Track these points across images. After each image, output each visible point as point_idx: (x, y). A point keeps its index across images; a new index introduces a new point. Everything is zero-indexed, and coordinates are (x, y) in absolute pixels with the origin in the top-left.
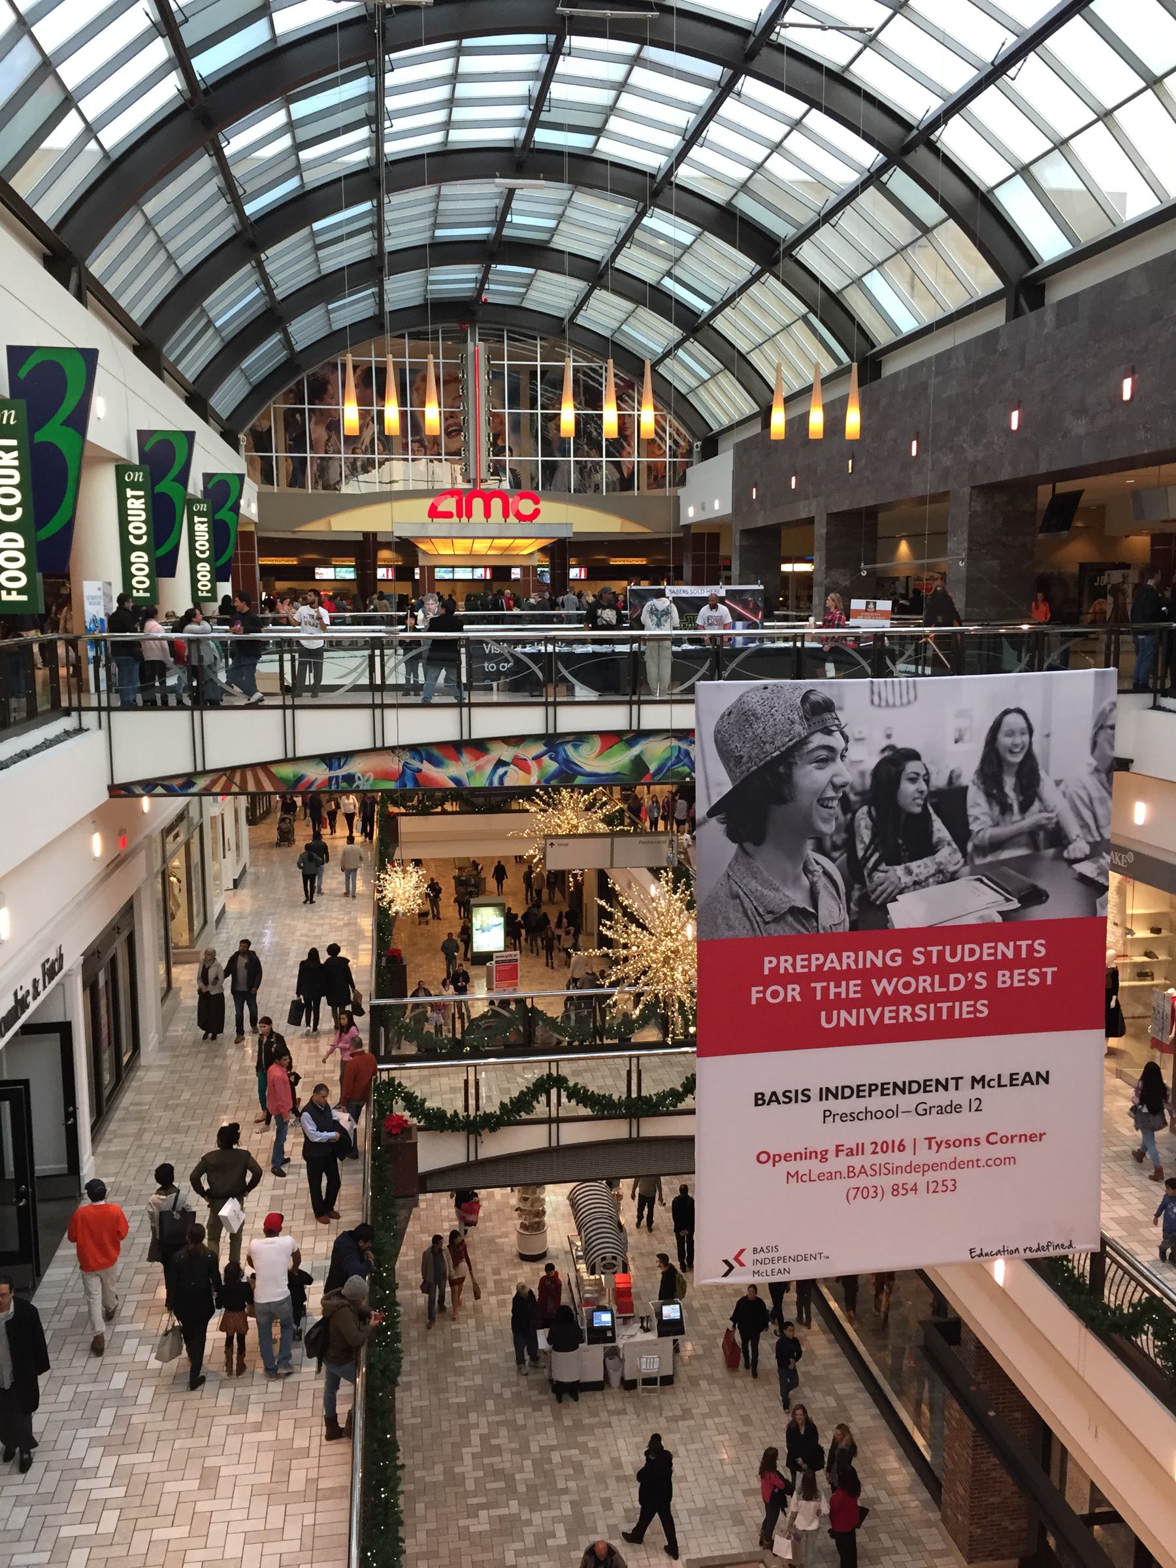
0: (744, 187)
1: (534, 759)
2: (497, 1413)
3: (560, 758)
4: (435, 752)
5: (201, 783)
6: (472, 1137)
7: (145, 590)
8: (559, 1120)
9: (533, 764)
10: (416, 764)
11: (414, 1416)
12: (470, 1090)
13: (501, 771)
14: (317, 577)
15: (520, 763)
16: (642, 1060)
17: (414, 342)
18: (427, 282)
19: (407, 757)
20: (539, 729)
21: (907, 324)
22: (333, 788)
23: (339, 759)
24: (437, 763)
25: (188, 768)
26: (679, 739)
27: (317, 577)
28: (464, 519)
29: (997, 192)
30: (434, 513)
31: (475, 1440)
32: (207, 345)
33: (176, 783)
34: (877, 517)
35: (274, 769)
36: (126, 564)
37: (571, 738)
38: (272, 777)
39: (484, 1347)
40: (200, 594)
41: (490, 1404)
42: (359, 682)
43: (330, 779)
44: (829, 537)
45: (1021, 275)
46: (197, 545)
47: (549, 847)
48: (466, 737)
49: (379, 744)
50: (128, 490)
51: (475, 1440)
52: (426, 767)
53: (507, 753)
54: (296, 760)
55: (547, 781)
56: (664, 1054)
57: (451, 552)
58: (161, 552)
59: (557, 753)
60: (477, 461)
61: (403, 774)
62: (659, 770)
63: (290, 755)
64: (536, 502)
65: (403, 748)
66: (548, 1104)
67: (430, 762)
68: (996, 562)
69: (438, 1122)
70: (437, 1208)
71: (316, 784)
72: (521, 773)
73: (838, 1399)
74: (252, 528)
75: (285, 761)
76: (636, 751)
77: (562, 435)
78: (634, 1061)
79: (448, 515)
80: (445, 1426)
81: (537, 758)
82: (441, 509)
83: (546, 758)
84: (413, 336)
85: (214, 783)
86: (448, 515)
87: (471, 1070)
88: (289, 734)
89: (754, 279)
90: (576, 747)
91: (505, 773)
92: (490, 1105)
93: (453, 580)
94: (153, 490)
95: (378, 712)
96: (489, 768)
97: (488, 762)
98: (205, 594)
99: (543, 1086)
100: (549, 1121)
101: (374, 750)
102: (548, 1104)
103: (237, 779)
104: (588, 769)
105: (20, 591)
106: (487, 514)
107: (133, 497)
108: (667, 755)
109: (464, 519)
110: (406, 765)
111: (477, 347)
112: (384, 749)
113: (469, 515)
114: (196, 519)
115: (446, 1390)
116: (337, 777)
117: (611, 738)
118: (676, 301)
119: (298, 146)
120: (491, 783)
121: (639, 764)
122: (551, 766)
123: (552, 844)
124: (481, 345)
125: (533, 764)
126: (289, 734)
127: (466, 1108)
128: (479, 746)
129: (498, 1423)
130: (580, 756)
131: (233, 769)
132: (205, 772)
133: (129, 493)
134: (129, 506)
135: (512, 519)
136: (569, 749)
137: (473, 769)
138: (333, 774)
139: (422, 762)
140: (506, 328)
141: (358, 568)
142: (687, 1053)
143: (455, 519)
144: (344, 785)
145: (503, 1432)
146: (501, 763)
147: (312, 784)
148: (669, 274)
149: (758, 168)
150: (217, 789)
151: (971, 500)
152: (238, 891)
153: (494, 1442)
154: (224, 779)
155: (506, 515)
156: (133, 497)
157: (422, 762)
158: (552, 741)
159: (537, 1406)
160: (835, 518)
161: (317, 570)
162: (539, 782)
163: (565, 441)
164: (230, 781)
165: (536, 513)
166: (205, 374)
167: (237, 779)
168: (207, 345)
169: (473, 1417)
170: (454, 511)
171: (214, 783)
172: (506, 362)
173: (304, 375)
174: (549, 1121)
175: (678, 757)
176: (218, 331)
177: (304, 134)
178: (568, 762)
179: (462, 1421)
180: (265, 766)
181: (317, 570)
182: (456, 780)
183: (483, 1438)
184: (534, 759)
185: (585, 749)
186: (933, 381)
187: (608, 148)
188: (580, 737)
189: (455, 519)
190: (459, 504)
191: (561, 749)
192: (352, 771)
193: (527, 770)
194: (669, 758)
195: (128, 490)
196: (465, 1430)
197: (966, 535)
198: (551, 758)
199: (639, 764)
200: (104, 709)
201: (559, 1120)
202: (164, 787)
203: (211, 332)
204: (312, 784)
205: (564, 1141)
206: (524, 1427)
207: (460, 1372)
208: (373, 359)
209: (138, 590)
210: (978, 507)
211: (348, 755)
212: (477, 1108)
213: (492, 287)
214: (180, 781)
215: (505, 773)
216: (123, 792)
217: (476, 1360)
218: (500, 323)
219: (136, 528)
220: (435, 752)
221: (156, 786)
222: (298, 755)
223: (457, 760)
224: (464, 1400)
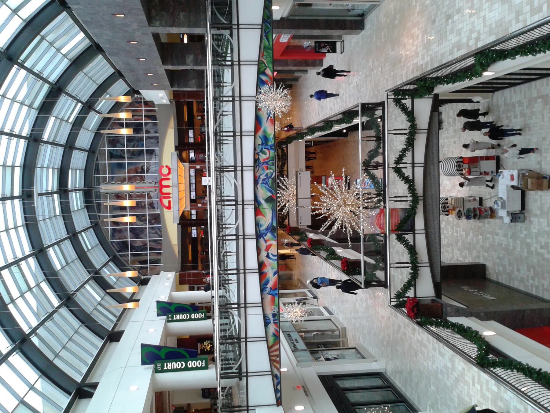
0: (30, 106)
1: (266, 243)
2: (532, 239)
3: (266, 232)
4: (263, 282)
5: (276, 372)
6: (417, 131)
7: (202, 362)
8: (413, 163)
9: (268, 243)
10: (268, 290)
11: (530, 271)
12: (398, 132)
13: (271, 256)
14: (196, 236)
15: (268, 248)
16: (391, 263)
17: (101, 172)
18: (78, 210)
19: (265, 293)
20: (254, 241)
21: (82, 35)
22: (278, 322)
23: (266, 319)
24: (268, 282)
25: (270, 377)
26: (258, 183)
27: (196, 236)
28: (171, 195)
29: (24, 18)
30: (169, 208)
31: (542, 251)
32: (108, 302)
33: (276, 381)
34: (163, 43)
35: (270, 344)
36: (192, 369)
37: (257, 228)
38: (273, 345)
39: (505, 236)
40: (204, 366)
41: (529, 241)
42: (237, 314)
43: (274, 323)
44: (173, 64)
45: (59, 5)
46: (185, 318)
47: (302, 224)
48: (257, 271)
49: (261, 305)
50: (164, 369)
51: (542, 251)
52: (270, 285)
53: (264, 254)
54: (266, 337)
55: (275, 237)
56: (387, 109)
57: (184, 198)
58: (187, 356)
59: (264, 233)
60: (148, 187)
61: (272, 294)
62: (271, 192)
63: (265, 339)
64: (163, 167)
65: (262, 295)
66: (406, 168)
67: (267, 284)
68: (181, 14)
69: (412, 283)
70: (448, 235)
71: (276, 328)
72: (272, 248)
73: (539, 97)
74: (178, 274)
75: (267, 340)
76: (263, 202)
77: (135, 205)
78: (392, 266)
79: (169, 202)
80: (535, 261)
81: (266, 241)
82: (167, 205)
83: (266, 238)
84: (99, 211)
85: (276, 367)
86: (169, 202)
87: (390, 132)
88: (257, 339)
89: (67, 94)
90: (261, 226)
91: (272, 254)
92: (406, 257)
93: (195, 184)
94: (164, 359)
95: (246, 237)
96: (270, 261)
97: (267, 261)
98: (204, 363)
99: (398, 171)
100: (413, 167)
101: (263, 306)
102: (406, 168)
103: (274, 358)
104: (270, 221)
105: (202, 362)
106: (168, 186)
107: (167, 367)
108: (264, 189)
109: (171, 195)
110: (268, 294)
111: (104, 188)
112: (262, 303)
113: (169, 194)
114: (175, 319)
115: (521, 256)
116: (273, 320)
117: (258, 212)
118: (79, 114)
119: (30, 289)
120: (276, 260)
121: (269, 200)
122: (269, 235)
123: (301, 223)
124: (101, 186)
125: (268, 243)
126: (257, 339)
127: (405, 134)
128: (261, 265)
129: (537, 239)
130: (265, 224)
131: (270, 360)
132: (272, 371)
133: (165, 368)
134: (170, 368)
135: (170, 177)
136: (262, 229)
137: (270, 267)
138: (272, 322)
139: (267, 287)
140: (93, 175)
141: (192, 226)
142: (387, 112)
143: (171, 199)
144: (276, 317)
145: (540, 239)
146: (268, 256)
147: (276, 330)
148: (67, 121)
149: (22, 104)
150: (278, 366)
151: (155, 26)
152: (318, 297)
153: (543, 244)
154: (274, 363)
155: (168, 179)
156: (167, 367)
157: (267, 287)
158: (258, 236)
159: (531, 222)
160: (164, 62)
161: (193, 236)
162: (275, 240)
163: (137, 203)
164: (275, 361)
165: (167, 166)
166: (117, 299)
167: (274, 358)
168: (108, 302)
169: (533, 249)
170: (168, 199)
171: (276, 367)
172: (107, 175)
173: (117, 254)
174: (413, 167)
175: (265, 184)
176: (102, 299)
177: (24, 287)
178: (267, 229)
179: (534, 253)
180: (269, 348)
181: (193, 236)
182: (275, 274)
183: (542, 247)
184: (266, 243)
185: (262, 222)
186: (105, 38)
187: (19, 161)
188: (257, 224)
189: (171, 199)
190: (165, 198)
191: (262, 232)
192: (271, 315)
193: (270, 246)
194: (265, 187)
195: (164, 369)
196: (538, 254)
197: (170, 28)
198: (266, 236)
199: (269, 200)
200: (248, 408)
201: (413, 163)
202: (277, 386)
203: (103, 302)
204: (276, 330)
205: (422, 160)
206: (539, 230)
207: (514, 249)
208: (109, 227)
209: (202, 365)
210: (158, 23)
211: (265, 316)
212: (407, 263)
213: (78, 194)
214: (275, 379)
215: (272, 254)
216: (280, 400)
217: (511, 240)
218: (92, 178)
219: (179, 366)
220: (263, 282)
221: (277, 388)
222: (265, 336)
223: (266, 274)
224: (526, 250)
